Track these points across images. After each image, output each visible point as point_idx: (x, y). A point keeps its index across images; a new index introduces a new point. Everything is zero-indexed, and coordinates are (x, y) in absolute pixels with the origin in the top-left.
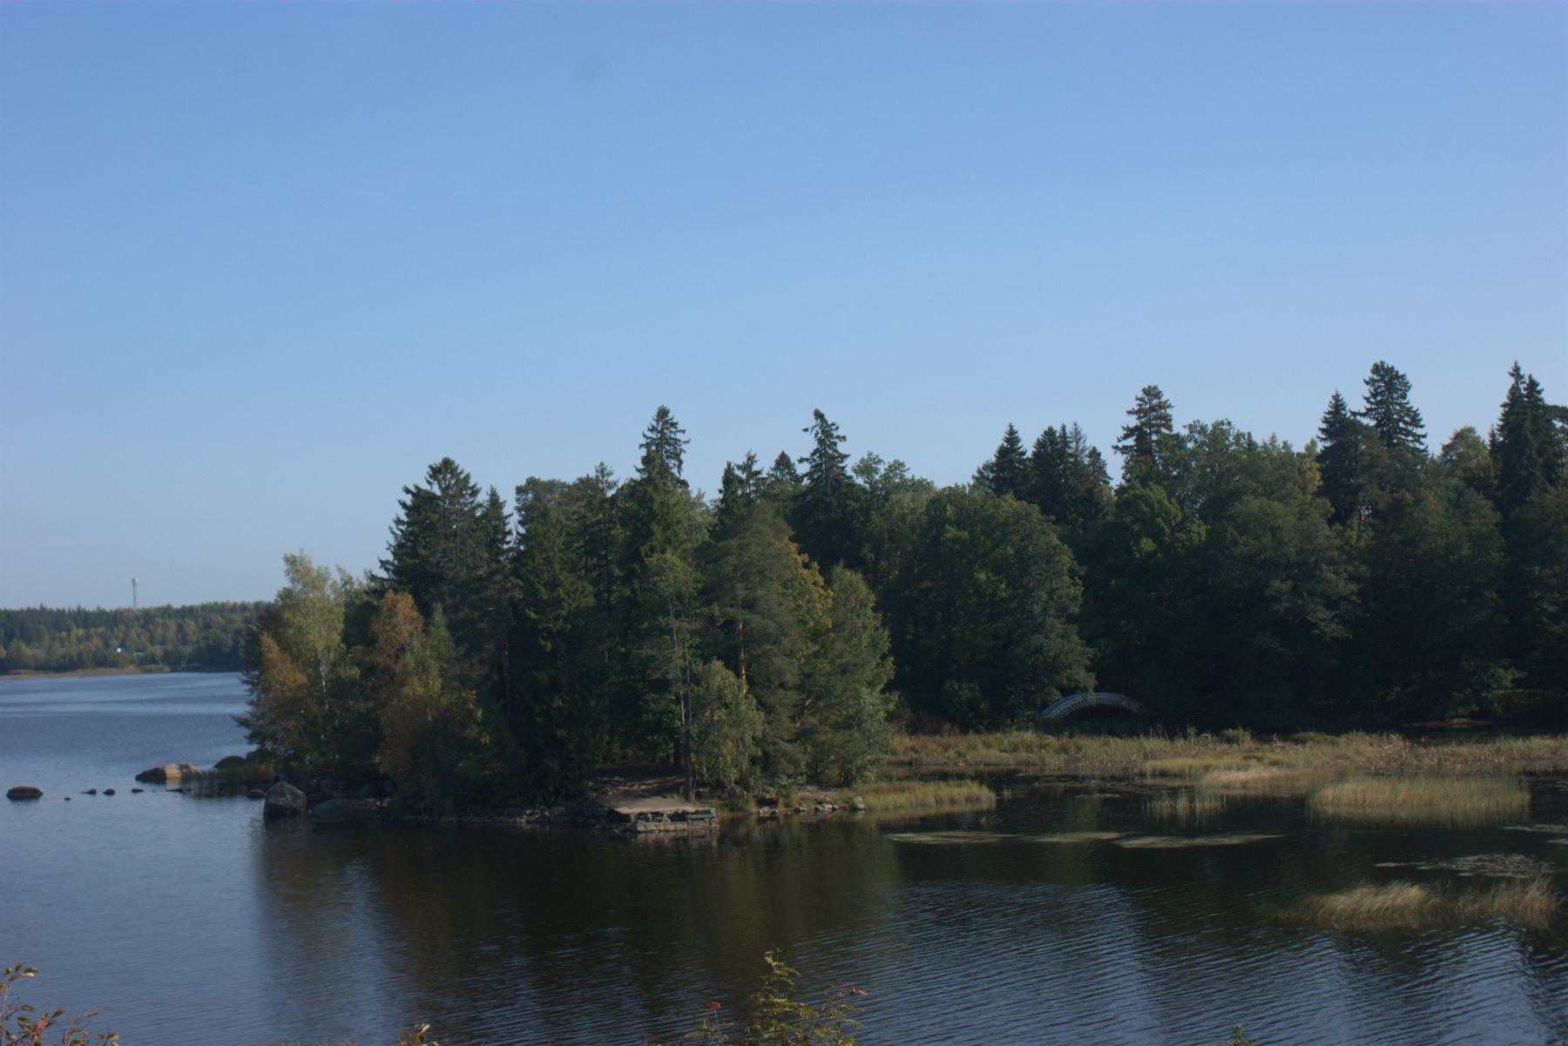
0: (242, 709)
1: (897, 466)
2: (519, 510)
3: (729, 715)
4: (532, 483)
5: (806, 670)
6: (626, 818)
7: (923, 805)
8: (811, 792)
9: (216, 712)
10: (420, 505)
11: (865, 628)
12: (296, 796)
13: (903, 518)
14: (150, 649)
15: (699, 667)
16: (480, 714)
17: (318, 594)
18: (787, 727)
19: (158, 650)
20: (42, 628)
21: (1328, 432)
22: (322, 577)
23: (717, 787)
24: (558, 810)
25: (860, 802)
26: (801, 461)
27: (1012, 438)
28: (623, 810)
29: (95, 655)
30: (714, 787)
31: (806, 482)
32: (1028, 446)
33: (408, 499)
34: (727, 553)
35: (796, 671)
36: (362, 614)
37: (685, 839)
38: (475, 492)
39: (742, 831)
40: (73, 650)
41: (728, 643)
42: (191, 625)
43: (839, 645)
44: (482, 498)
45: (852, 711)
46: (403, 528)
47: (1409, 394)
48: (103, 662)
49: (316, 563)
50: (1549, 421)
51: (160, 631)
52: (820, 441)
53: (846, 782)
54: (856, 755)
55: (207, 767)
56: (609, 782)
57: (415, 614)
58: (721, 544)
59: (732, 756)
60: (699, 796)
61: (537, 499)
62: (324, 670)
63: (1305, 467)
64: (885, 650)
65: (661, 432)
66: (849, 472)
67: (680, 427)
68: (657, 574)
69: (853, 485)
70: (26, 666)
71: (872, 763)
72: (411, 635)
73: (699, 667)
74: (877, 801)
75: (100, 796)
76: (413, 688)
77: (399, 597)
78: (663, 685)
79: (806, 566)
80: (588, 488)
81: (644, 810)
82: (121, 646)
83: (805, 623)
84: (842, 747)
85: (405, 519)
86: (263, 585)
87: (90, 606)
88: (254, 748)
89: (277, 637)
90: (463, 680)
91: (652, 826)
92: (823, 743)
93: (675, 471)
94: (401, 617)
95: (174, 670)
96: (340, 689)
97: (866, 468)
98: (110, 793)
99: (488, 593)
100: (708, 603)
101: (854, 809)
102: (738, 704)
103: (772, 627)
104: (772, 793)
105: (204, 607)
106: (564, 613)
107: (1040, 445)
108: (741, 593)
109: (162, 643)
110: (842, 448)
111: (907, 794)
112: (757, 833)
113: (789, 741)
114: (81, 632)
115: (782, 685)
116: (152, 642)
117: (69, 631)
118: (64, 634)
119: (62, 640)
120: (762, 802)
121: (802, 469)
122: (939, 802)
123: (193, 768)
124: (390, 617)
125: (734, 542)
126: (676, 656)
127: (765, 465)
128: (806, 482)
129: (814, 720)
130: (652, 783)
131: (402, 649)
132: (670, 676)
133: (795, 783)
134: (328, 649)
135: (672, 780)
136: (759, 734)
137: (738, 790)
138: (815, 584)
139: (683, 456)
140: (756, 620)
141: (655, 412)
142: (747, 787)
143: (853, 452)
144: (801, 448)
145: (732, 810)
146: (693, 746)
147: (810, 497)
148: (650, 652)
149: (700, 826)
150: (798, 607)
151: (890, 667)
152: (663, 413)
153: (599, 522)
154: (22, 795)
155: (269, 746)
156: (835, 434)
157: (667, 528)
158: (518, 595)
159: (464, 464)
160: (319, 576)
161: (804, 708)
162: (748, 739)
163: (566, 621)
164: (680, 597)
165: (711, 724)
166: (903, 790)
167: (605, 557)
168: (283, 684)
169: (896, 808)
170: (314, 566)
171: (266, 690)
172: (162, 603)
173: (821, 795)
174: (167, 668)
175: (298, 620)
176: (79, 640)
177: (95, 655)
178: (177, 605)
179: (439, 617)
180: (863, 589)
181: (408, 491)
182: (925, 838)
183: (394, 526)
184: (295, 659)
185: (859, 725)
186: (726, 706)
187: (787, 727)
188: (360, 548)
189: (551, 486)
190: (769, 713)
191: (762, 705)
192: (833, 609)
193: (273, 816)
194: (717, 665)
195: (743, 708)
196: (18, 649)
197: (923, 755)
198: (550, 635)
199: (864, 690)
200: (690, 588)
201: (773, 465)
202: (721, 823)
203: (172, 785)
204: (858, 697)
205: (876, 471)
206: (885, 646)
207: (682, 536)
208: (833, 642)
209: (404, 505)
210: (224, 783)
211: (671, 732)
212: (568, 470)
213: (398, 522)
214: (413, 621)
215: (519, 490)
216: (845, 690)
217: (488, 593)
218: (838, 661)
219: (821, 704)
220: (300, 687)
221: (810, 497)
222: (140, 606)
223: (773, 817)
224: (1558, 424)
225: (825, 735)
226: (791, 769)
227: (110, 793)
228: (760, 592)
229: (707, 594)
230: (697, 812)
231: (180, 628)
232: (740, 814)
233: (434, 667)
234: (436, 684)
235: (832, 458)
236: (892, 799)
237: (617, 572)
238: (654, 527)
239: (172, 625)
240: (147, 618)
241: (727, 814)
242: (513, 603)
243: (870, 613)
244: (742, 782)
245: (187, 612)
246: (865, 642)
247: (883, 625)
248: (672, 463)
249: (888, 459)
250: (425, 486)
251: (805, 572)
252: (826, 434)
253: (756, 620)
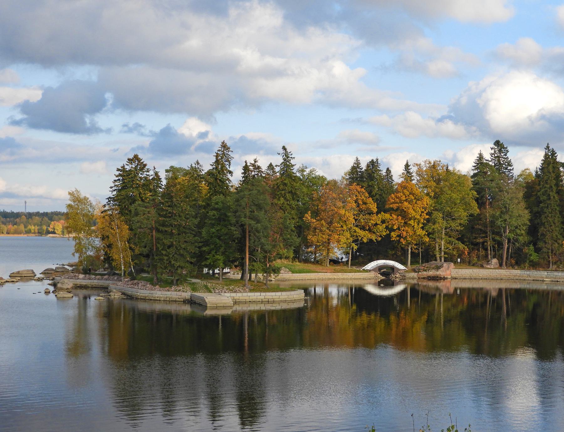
21: (476, 168)
26: (276, 166)
27: (358, 163)
32: (363, 166)
47: (508, 154)
49: (83, 195)
50: (558, 168)
52: (285, 160)
63: (444, 190)
93: (227, 167)
107: (368, 166)
110: (292, 162)
121: (277, 169)
143: (297, 163)
144: (278, 160)
178: (41, 211)
190: (500, 151)
222: (27, 211)
224: (561, 169)
235: (288, 166)
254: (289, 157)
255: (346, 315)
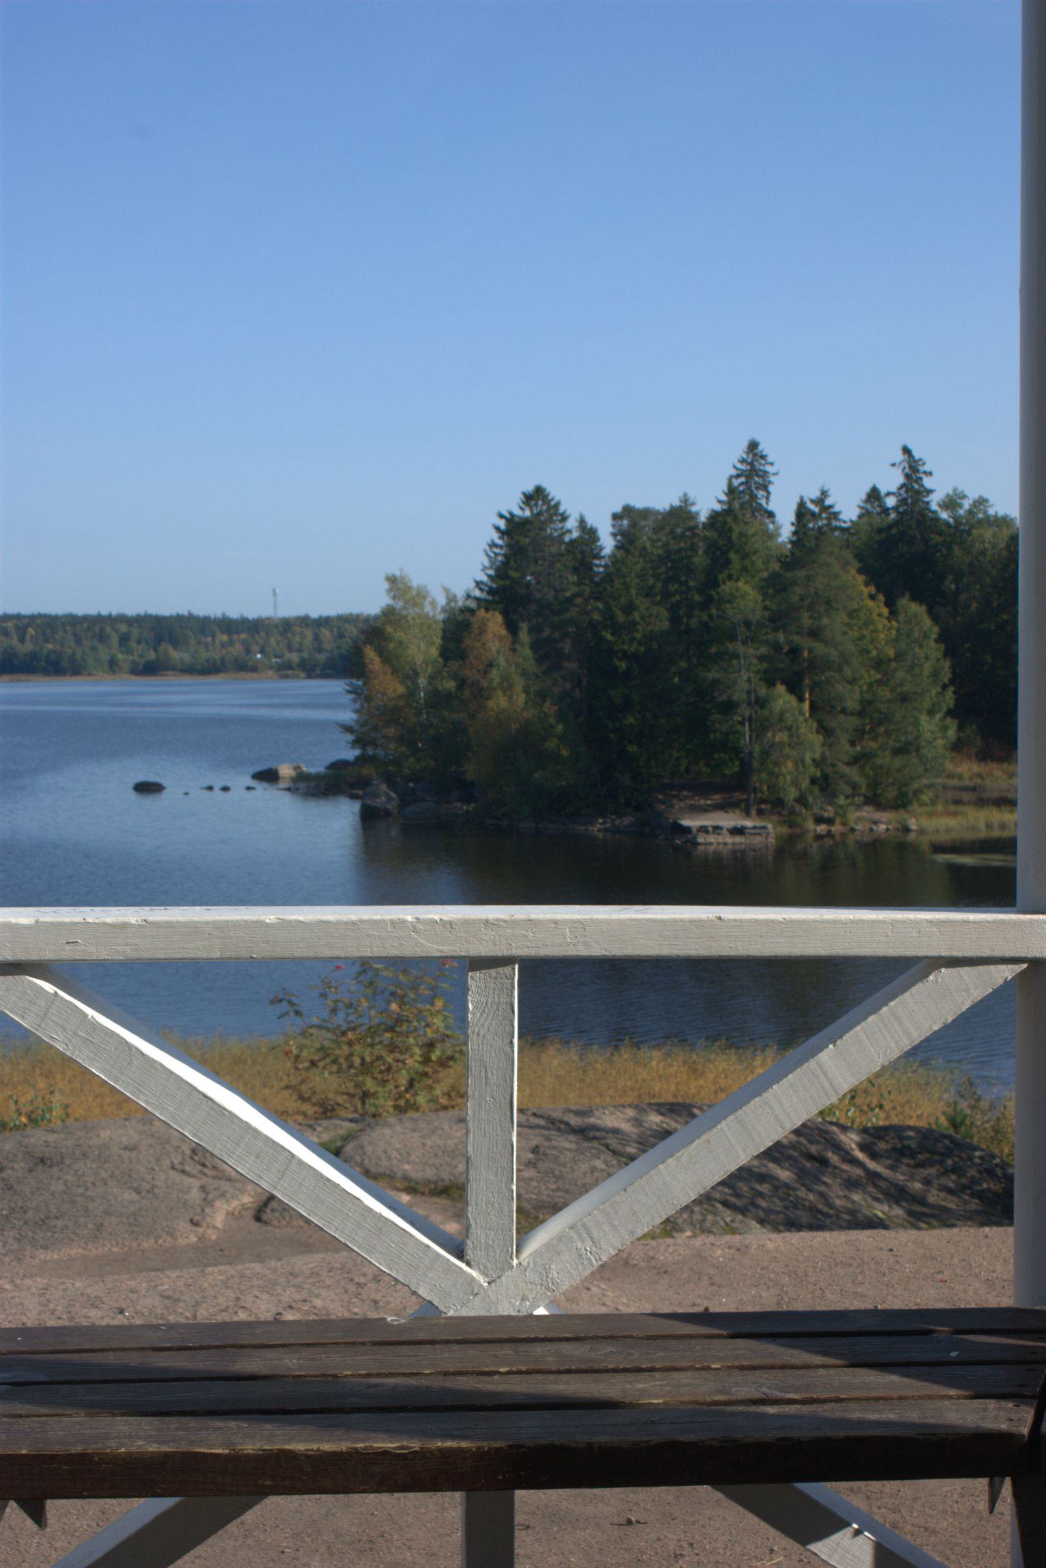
0: (349, 716)
1: (981, 502)
2: (614, 535)
3: (791, 736)
4: (628, 511)
5: (867, 697)
6: (687, 830)
7: (973, 829)
8: (868, 812)
9: (324, 714)
10: (514, 529)
11: (927, 658)
12: (389, 799)
13: (983, 553)
14: (288, 656)
15: (763, 691)
16: (560, 727)
17: (417, 610)
18: (846, 749)
19: (294, 657)
20: (190, 633)
22: (422, 595)
23: (778, 804)
24: (627, 821)
25: (913, 824)
26: (888, 494)
28: (686, 822)
29: (236, 660)
30: (775, 805)
31: (893, 516)
33: (502, 524)
34: (794, 583)
35: (857, 696)
36: (458, 629)
37: (743, 852)
38: (564, 518)
39: (799, 846)
40: (216, 655)
41: (793, 672)
42: (326, 634)
43: (900, 674)
44: (571, 524)
45: (911, 738)
46: (497, 551)
48: (243, 667)
51: (297, 639)
52: (907, 476)
53: (902, 803)
54: (912, 779)
55: (320, 769)
56: (674, 797)
57: (504, 632)
58: (789, 574)
59: (791, 777)
60: (760, 813)
61: (633, 525)
62: (422, 681)
64: (946, 680)
65: (751, 464)
66: (934, 507)
67: (770, 459)
68: (729, 602)
69: (937, 519)
70: (174, 669)
71: (930, 786)
72: (498, 652)
73: (763, 691)
74: (929, 824)
75: (217, 792)
76: (500, 701)
77: (489, 615)
78: (729, 707)
79: (872, 597)
80: (681, 514)
81: (720, 824)
82: (261, 652)
83: (869, 652)
84: (899, 770)
85: (500, 542)
86: (370, 601)
87: (234, 614)
88: (357, 752)
89: (380, 651)
90: (543, 695)
91: (711, 838)
92: (881, 767)
93: (763, 502)
94: (490, 635)
95: (309, 677)
96: (438, 700)
97: (951, 503)
98: (225, 789)
99: (568, 615)
100: (775, 630)
101: (907, 830)
102: (798, 727)
103: (833, 654)
104: (829, 812)
105: (340, 618)
106: (638, 636)
108: (806, 622)
109: (300, 650)
110: (928, 482)
111: (959, 818)
112: (815, 848)
113: (848, 764)
114: (225, 638)
115: (843, 711)
116: (290, 649)
117: (214, 636)
118: (209, 639)
119: (207, 646)
120: (819, 820)
121: (891, 502)
122: (989, 826)
123: (304, 769)
124: (480, 634)
125: (801, 574)
126: (742, 677)
127: (495, 537)
128: (893, 516)
129: (873, 745)
130: (717, 798)
131: (491, 665)
132: (735, 698)
133: (852, 804)
134: (426, 662)
135: (738, 796)
136: (817, 756)
137: (798, 808)
138: (880, 615)
139: (771, 488)
140: (820, 648)
141: (745, 445)
142: (806, 806)
143: (938, 488)
145: (790, 826)
146: (756, 764)
147: (894, 531)
148: (717, 675)
149: (757, 840)
150: (862, 637)
151: (949, 697)
152: (753, 446)
153: (680, 550)
154: (146, 788)
155: (370, 751)
156: (922, 469)
157: (744, 558)
158: (596, 617)
159: (555, 492)
160: (419, 594)
161: (863, 732)
162: (808, 761)
163: (640, 643)
164: (747, 624)
165: (772, 746)
166: (955, 814)
167: (686, 583)
168: (384, 694)
169: (948, 830)
170: (414, 584)
171: (368, 699)
172: (300, 612)
173: (878, 816)
174: (303, 674)
175: (399, 635)
176: (223, 645)
177: (236, 660)
178: (314, 615)
179: (524, 636)
180: (927, 621)
181: (501, 516)
182: (967, 860)
183: (487, 548)
184: (395, 671)
185: (918, 750)
186: (789, 729)
187: (846, 749)
188: (455, 566)
189: (646, 513)
191: (823, 729)
192: (896, 640)
193: (369, 817)
194: (780, 689)
195: (802, 730)
196: (166, 652)
197: (988, 781)
198: (625, 656)
199: (924, 718)
200: (758, 615)
201: (864, 497)
202: (777, 838)
203: (282, 785)
204: (916, 723)
205: (960, 506)
206: (946, 676)
207: (759, 565)
208: (894, 671)
209: (497, 529)
210: (324, 785)
211: (737, 751)
212: (659, 498)
213: (493, 545)
214: (501, 639)
215: (616, 517)
216: (904, 717)
217: (568, 615)
218: (899, 690)
219: (882, 729)
220: (399, 697)
221: (894, 531)
223: (829, 835)
225: (884, 759)
226: (848, 790)
227: (225, 789)
228: (825, 621)
229: (778, 620)
230: (754, 828)
231: (317, 637)
232: (798, 831)
233: (519, 683)
234: (521, 699)
235: (918, 493)
236: (952, 822)
237: (697, 598)
238: (733, 556)
239: (309, 634)
240: (287, 626)
241: (785, 830)
242: (593, 626)
243: (932, 644)
244: (801, 800)
245: (324, 622)
246: (926, 673)
247: (945, 656)
248: (761, 493)
249: (972, 494)
250: (518, 512)
251: (871, 603)
252: (913, 469)
253: (820, 648)
254: (918, 471)
255: (216, 1429)
